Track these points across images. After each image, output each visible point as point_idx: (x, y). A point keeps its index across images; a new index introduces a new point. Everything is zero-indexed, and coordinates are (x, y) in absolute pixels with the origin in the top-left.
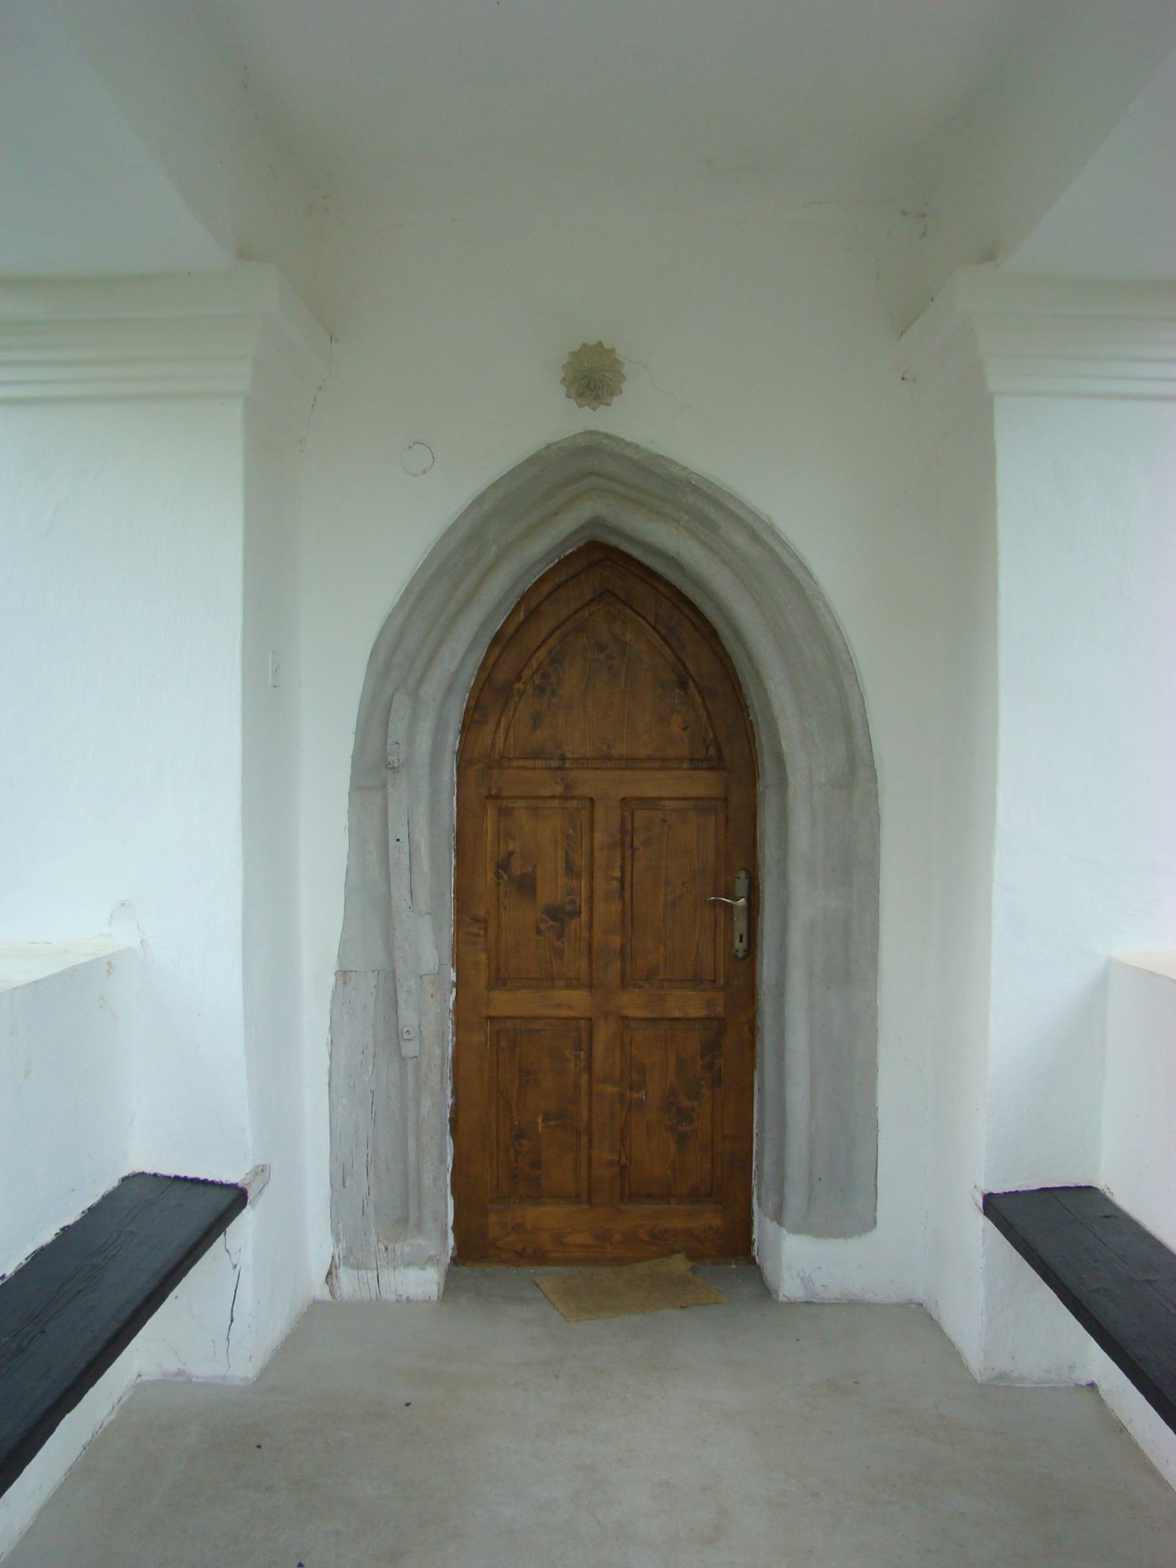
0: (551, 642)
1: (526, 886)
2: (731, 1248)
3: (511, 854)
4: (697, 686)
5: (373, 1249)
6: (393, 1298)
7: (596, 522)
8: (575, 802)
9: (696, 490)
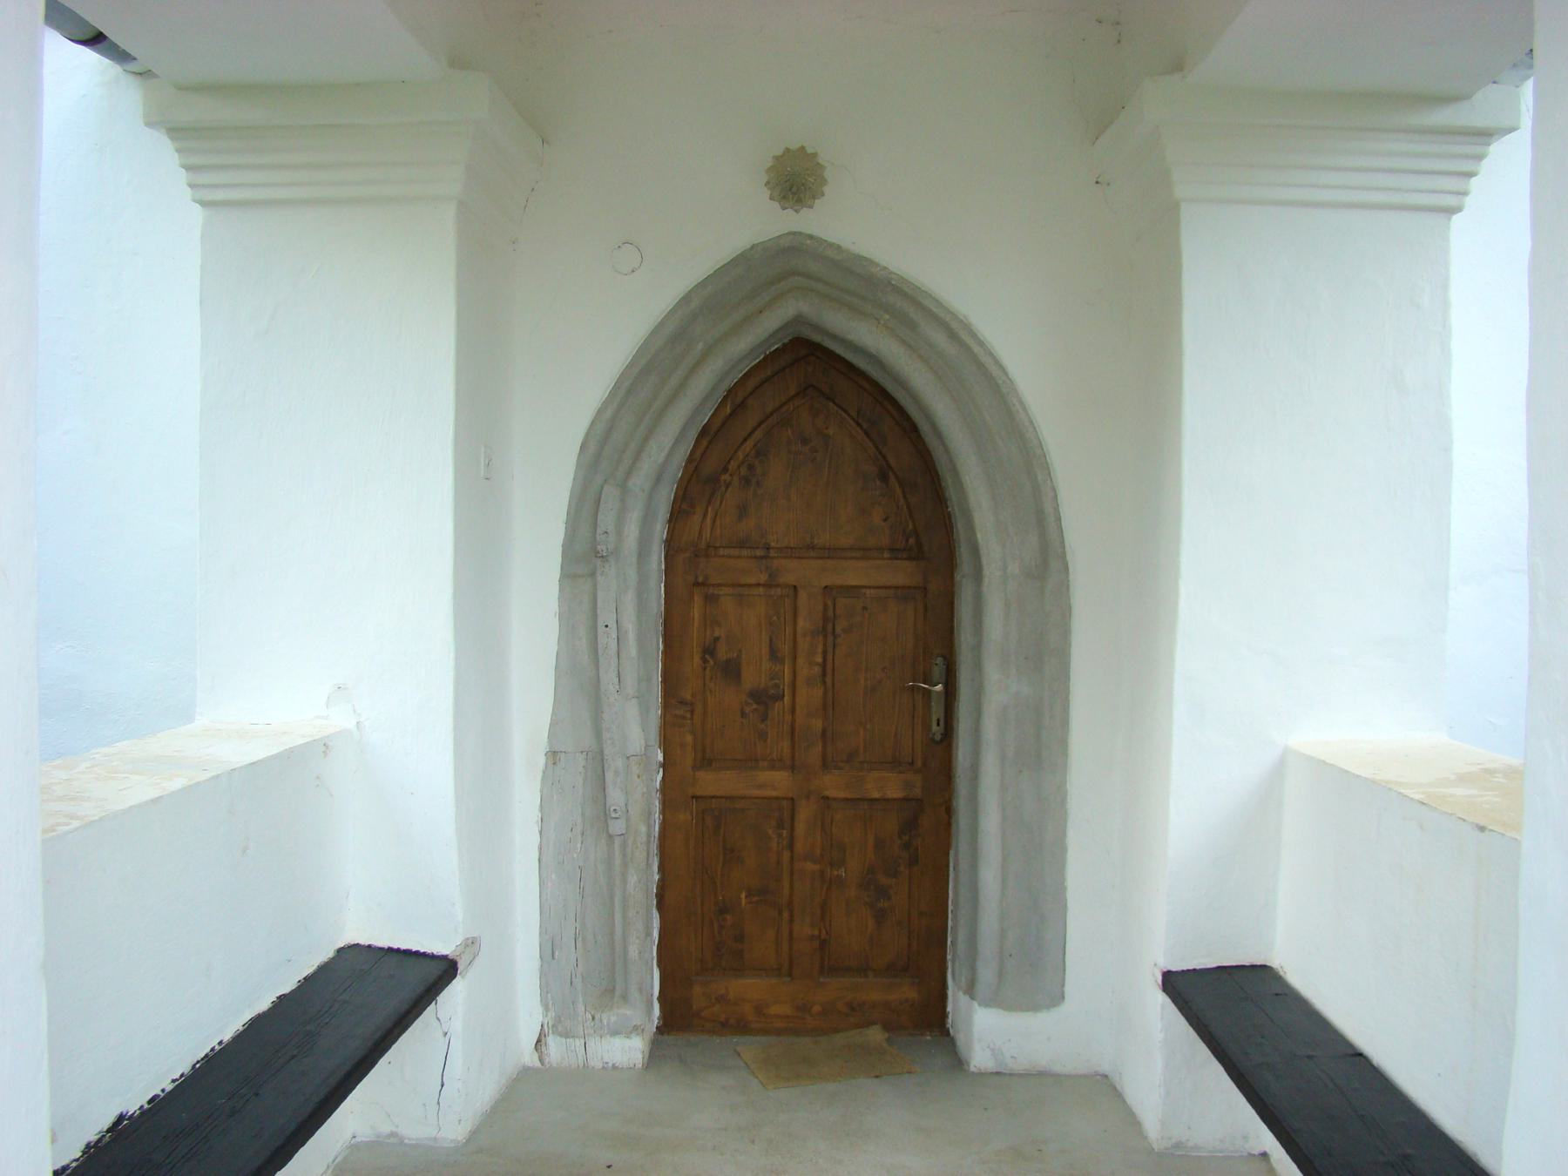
0: (759, 434)
1: (731, 671)
2: (926, 1021)
3: (717, 639)
4: (897, 477)
6: (599, 1065)
7: (799, 320)
9: (897, 290)
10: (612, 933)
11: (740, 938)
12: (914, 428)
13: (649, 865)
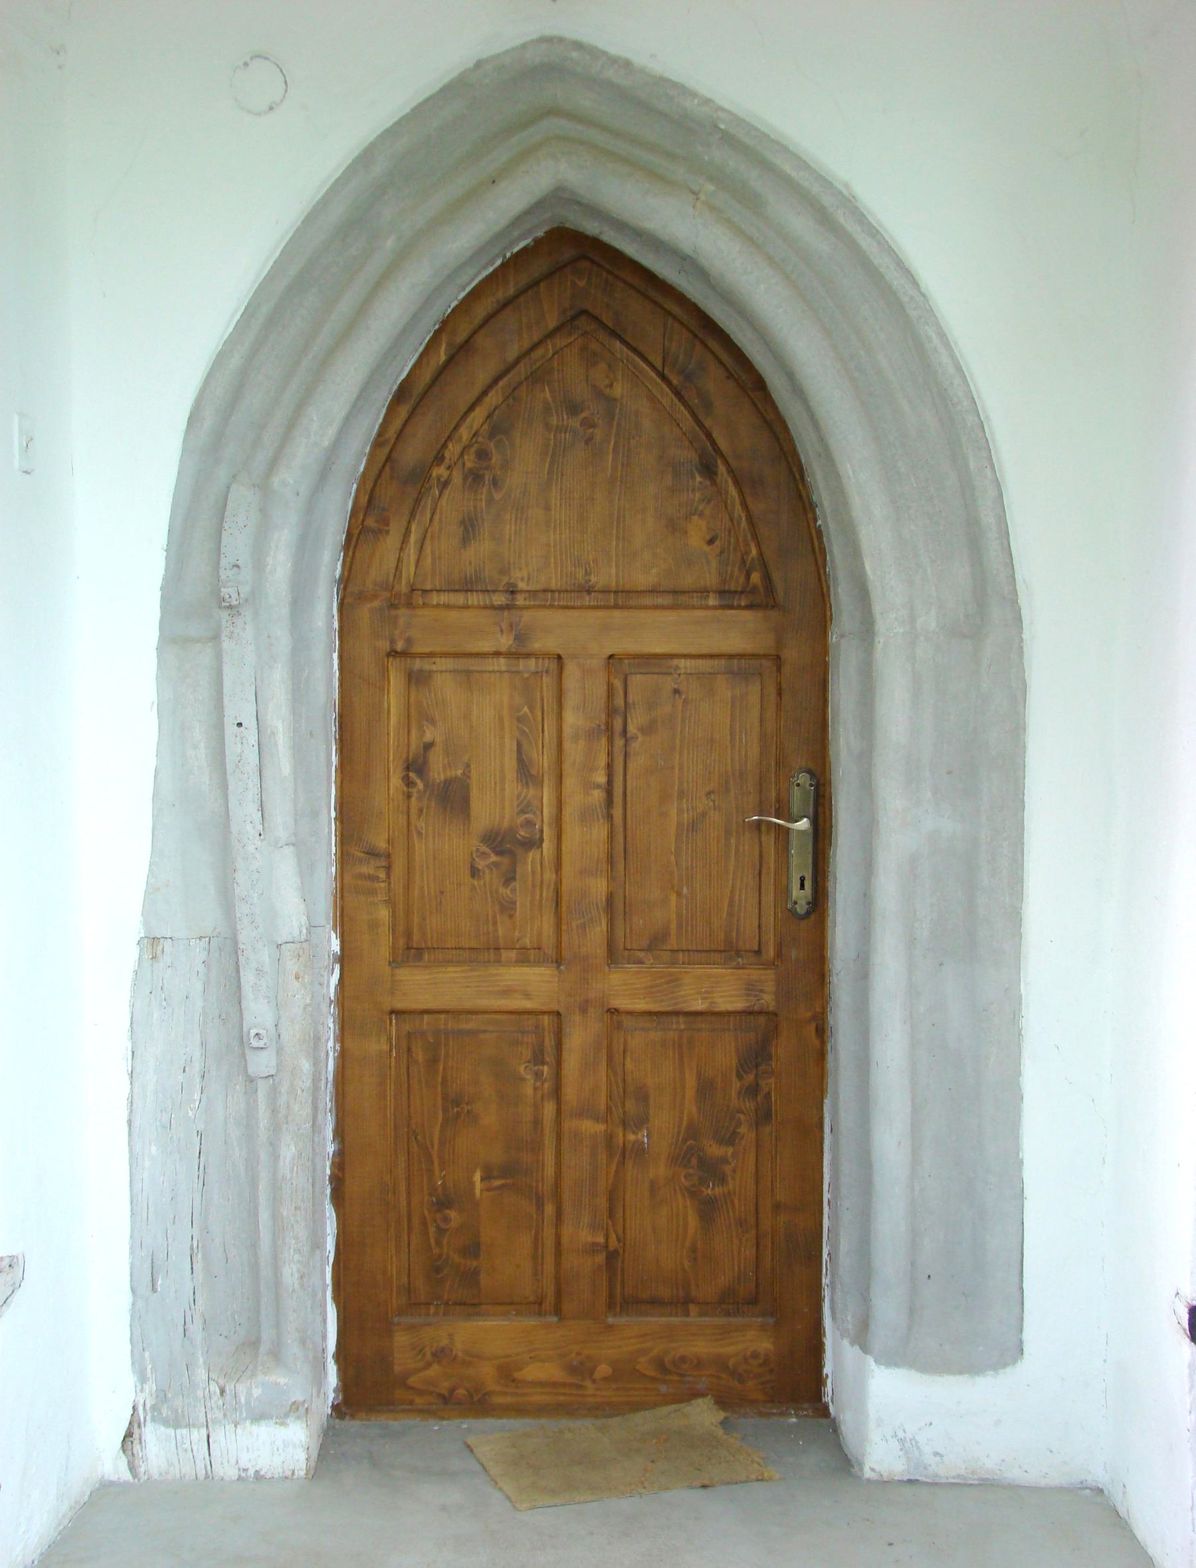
0: (493, 399)
1: (454, 799)
2: (794, 1387)
3: (428, 746)
4: (731, 471)
5: (200, 1393)
6: (232, 1473)
7: (560, 196)
8: (532, 663)
9: (728, 139)
10: (254, 1246)
11: (473, 1249)
12: (760, 384)
13: (315, 1127)
